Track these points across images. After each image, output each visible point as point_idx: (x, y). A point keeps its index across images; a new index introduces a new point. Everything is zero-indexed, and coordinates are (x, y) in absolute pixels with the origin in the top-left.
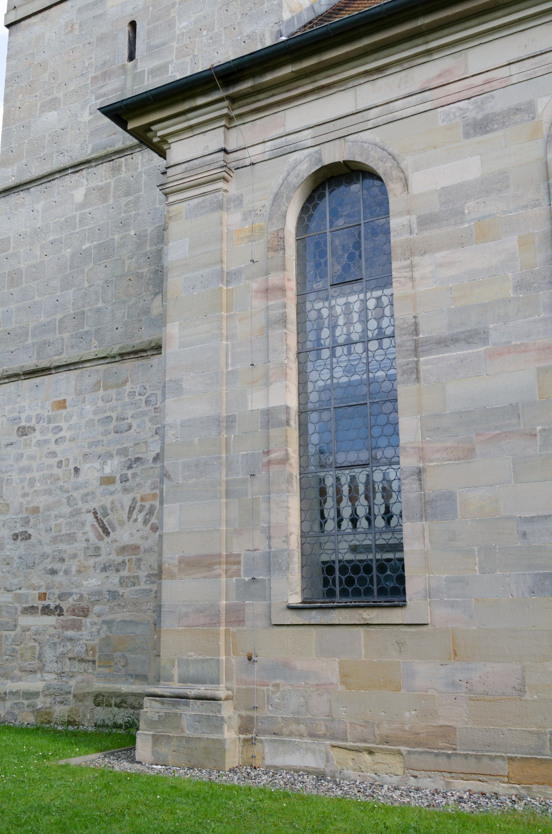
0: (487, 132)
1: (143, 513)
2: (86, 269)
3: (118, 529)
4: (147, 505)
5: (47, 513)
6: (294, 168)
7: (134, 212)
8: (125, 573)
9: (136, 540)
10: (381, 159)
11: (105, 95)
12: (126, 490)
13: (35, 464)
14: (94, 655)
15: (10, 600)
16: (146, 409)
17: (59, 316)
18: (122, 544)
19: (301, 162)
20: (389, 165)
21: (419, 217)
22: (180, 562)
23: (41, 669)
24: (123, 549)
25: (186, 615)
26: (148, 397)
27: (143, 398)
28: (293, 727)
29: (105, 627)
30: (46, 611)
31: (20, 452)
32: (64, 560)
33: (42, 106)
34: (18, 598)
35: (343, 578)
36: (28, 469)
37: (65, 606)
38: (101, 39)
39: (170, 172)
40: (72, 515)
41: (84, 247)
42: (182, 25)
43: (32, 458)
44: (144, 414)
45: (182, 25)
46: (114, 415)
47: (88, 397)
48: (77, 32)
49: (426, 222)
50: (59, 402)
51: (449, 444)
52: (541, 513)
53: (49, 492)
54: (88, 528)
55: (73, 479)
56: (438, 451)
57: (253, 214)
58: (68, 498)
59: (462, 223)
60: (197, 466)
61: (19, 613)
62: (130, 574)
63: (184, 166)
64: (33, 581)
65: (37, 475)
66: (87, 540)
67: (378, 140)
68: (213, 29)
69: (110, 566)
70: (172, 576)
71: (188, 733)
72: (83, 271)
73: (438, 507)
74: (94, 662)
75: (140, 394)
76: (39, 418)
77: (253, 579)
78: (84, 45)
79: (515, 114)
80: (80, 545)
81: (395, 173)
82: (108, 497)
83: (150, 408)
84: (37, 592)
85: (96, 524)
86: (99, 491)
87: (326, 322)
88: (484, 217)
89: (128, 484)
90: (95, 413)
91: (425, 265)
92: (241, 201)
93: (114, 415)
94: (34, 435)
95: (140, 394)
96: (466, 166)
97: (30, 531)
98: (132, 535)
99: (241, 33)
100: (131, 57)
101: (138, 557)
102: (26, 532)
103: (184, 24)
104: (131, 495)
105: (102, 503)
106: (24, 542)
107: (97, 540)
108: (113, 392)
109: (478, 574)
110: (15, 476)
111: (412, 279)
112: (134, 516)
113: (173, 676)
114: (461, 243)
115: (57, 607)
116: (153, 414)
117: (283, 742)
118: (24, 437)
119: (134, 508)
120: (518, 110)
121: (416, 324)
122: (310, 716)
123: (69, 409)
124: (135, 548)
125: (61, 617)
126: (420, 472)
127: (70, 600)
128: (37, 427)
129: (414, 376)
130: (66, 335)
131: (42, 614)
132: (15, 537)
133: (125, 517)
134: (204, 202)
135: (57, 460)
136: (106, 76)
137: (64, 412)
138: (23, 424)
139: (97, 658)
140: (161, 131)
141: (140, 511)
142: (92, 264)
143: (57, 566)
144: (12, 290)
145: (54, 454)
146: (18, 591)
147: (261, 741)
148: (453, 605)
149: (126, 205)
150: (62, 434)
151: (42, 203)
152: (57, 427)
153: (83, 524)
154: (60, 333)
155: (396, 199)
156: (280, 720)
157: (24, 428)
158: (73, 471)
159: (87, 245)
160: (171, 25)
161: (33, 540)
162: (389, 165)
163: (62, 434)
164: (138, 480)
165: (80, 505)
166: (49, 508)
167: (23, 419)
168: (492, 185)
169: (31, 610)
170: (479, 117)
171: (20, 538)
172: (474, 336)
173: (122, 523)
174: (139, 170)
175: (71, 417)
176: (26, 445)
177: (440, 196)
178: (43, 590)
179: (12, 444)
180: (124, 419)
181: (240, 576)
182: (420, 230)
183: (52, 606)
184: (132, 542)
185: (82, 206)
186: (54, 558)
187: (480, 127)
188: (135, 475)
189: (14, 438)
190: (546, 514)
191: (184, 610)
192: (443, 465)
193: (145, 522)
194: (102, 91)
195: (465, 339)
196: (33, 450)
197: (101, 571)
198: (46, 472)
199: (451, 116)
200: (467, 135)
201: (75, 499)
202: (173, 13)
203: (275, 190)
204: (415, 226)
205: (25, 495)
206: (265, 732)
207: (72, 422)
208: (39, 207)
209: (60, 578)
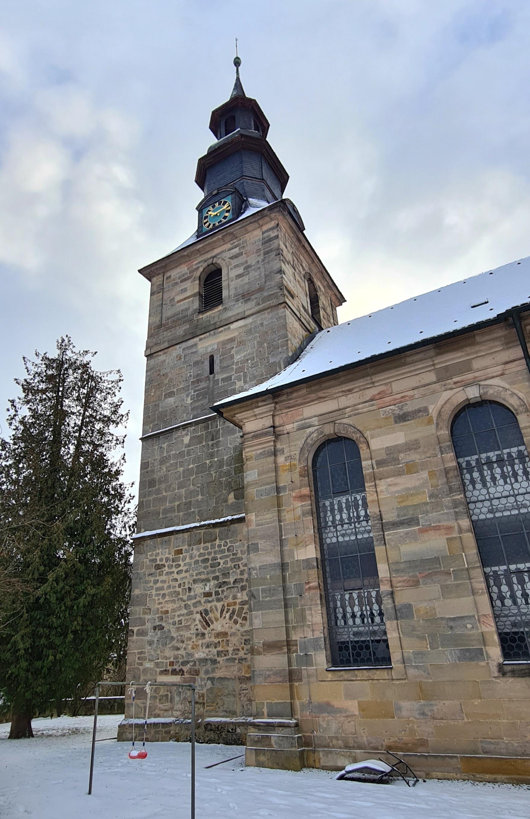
0: (406, 421)
1: (229, 614)
2: (192, 478)
3: (215, 622)
4: (231, 608)
5: (173, 614)
6: (310, 436)
7: (216, 449)
8: (220, 649)
9: (226, 629)
10: (354, 432)
11: (198, 390)
12: (218, 600)
13: (165, 586)
14: (203, 699)
15: (152, 666)
16: (228, 554)
17: (177, 503)
18: (218, 631)
19: (313, 433)
20: (358, 435)
21: (376, 461)
22: (264, 645)
23: (172, 709)
24: (218, 635)
25: (269, 676)
26: (229, 547)
27: (226, 548)
28: (335, 742)
29: (209, 682)
30: (174, 672)
31: (156, 579)
32: (184, 642)
33: (165, 395)
34: (157, 665)
35: (355, 652)
36: (162, 588)
37: (185, 669)
38: (196, 363)
39: (246, 437)
40: (187, 614)
41: (190, 467)
42: (237, 358)
43: (164, 582)
44: (227, 556)
45: (237, 358)
46: (210, 557)
47: (194, 547)
48: (183, 360)
49: (380, 463)
50: (178, 550)
51: (405, 578)
52: (459, 615)
53: (173, 601)
54: (197, 622)
55: (188, 594)
56: (400, 582)
57: (290, 458)
58: (185, 605)
59: (399, 464)
60: (270, 590)
61: (158, 673)
62: (223, 649)
63: (252, 434)
64: (166, 655)
65: (166, 592)
66: (197, 630)
67: (351, 423)
68: (254, 360)
69: (211, 645)
70: (259, 653)
71: (276, 747)
72: (190, 479)
73: (402, 613)
74: (204, 703)
75: (224, 546)
76: (167, 559)
77: (306, 654)
78: (187, 366)
79: (418, 413)
80: (193, 631)
81: (362, 439)
82: (208, 604)
83: (230, 553)
84: (168, 661)
85: (202, 620)
86: (203, 600)
87: (329, 508)
88: (410, 462)
89: (219, 596)
90: (199, 556)
91: (382, 485)
92: (283, 452)
93: (210, 557)
94: (164, 569)
95: (224, 546)
96: (398, 437)
97: (164, 624)
98: (223, 626)
99: (268, 362)
100: (212, 371)
101: (227, 639)
102: (161, 625)
103: (238, 357)
104: (222, 603)
105: (205, 608)
106: (159, 632)
107: (202, 630)
108: (209, 545)
109: (429, 649)
110: (154, 592)
111: (377, 492)
112: (224, 615)
113: (263, 713)
114: (400, 473)
115: (180, 671)
116: (232, 557)
117: (331, 752)
118: (159, 570)
119: (224, 611)
120: (419, 411)
121: (381, 515)
122: (344, 735)
123: (184, 554)
124: (225, 634)
125: (183, 676)
126: (392, 593)
127: (188, 665)
128: (166, 564)
129: (383, 542)
130: (181, 514)
131: (172, 674)
132: (155, 628)
133: (219, 615)
134: (264, 451)
135: (178, 583)
136: (198, 381)
137: (181, 556)
138: (158, 563)
139: (205, 701)
140: (239, 416)
141: (227, 612)
142: (194, 476)
143: (180, 645)
144: (150, 489)
145: (176, 580)
146: (157, 661)
147: (319, 751)
148: (417, 667)
149: (212, 445)
150: (180, 568)
151: (166, 444)
152: (178, 564)
153: (195, 620)
154: (178, 512)
155: (364, 452)
156: (327, 738)
157: (159, 565)
158: (187, 590)
159: (192, 466)
160: (232, 357)
161: (165, 629)
162: (358, 435)
163: (180, 568)
164: (225, 593)
165: (192, 609)
166: (174, 610)
167: (158, 560)
168: (412, 446)
169: (165, 672)
170: (401, 414)
171: (157, 629)
172: (412, 521)
173: (217, 620)
174: (218, 427)
175: (186, 559)
176: (160, 575)
177: (386, 451)
178: (172, 660)
179: (152, 574)
180: (215, 560)
181: (297, 653)
182: (377, 468)
183: (178, 669)
184: (223, 630)
185: (188, 445)
186: (178, 640)
187: (402, 418)
188: (223, 591)
189: (153, 570)
190: (462, 616)
191: (268, 673)
192: (403, 589)
193: (231, 618)
194: (197, 388)
195: (407, 523)
196: (164, 578)
197: (206, 648)
198: (172, 590)
199: (387, 413)
200: (396, 422)
201: (189, 606)
202: (233, 352)
203: (301, 446)
204: (375, 465)
205: (160, 603)
206: (320, 746)
207: (186, 561)
208: (165, 446)
209: (182, 652)
